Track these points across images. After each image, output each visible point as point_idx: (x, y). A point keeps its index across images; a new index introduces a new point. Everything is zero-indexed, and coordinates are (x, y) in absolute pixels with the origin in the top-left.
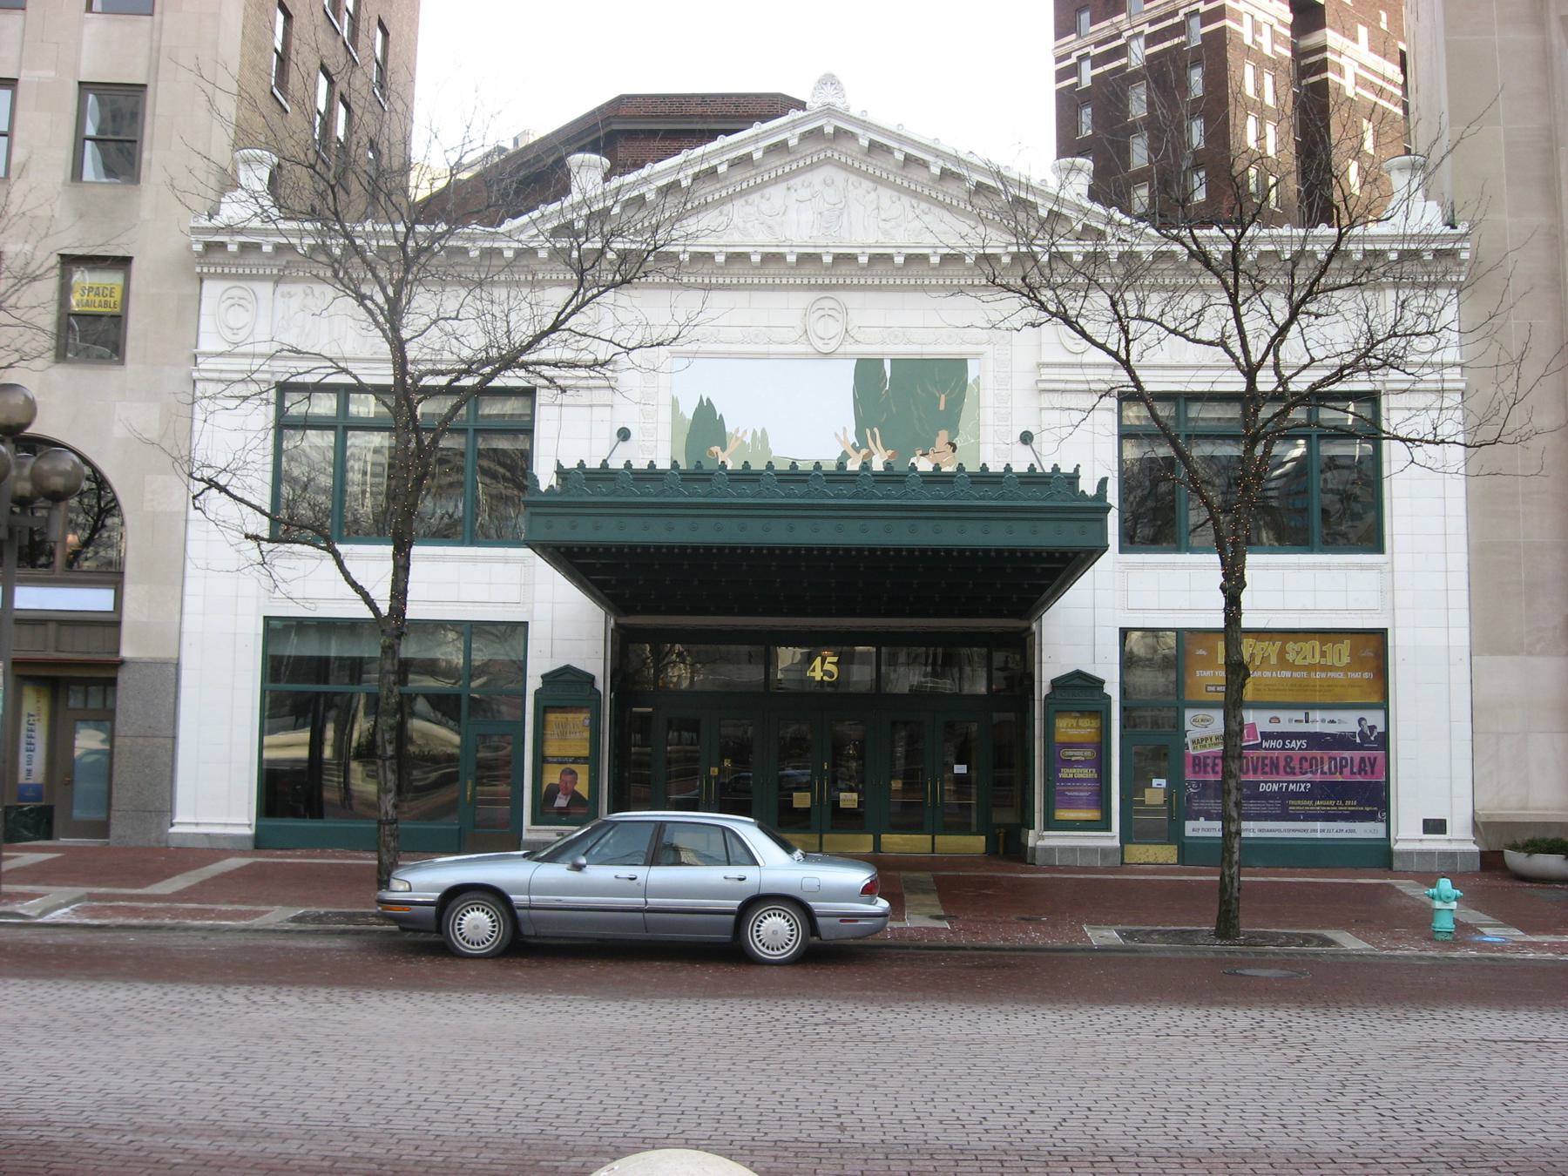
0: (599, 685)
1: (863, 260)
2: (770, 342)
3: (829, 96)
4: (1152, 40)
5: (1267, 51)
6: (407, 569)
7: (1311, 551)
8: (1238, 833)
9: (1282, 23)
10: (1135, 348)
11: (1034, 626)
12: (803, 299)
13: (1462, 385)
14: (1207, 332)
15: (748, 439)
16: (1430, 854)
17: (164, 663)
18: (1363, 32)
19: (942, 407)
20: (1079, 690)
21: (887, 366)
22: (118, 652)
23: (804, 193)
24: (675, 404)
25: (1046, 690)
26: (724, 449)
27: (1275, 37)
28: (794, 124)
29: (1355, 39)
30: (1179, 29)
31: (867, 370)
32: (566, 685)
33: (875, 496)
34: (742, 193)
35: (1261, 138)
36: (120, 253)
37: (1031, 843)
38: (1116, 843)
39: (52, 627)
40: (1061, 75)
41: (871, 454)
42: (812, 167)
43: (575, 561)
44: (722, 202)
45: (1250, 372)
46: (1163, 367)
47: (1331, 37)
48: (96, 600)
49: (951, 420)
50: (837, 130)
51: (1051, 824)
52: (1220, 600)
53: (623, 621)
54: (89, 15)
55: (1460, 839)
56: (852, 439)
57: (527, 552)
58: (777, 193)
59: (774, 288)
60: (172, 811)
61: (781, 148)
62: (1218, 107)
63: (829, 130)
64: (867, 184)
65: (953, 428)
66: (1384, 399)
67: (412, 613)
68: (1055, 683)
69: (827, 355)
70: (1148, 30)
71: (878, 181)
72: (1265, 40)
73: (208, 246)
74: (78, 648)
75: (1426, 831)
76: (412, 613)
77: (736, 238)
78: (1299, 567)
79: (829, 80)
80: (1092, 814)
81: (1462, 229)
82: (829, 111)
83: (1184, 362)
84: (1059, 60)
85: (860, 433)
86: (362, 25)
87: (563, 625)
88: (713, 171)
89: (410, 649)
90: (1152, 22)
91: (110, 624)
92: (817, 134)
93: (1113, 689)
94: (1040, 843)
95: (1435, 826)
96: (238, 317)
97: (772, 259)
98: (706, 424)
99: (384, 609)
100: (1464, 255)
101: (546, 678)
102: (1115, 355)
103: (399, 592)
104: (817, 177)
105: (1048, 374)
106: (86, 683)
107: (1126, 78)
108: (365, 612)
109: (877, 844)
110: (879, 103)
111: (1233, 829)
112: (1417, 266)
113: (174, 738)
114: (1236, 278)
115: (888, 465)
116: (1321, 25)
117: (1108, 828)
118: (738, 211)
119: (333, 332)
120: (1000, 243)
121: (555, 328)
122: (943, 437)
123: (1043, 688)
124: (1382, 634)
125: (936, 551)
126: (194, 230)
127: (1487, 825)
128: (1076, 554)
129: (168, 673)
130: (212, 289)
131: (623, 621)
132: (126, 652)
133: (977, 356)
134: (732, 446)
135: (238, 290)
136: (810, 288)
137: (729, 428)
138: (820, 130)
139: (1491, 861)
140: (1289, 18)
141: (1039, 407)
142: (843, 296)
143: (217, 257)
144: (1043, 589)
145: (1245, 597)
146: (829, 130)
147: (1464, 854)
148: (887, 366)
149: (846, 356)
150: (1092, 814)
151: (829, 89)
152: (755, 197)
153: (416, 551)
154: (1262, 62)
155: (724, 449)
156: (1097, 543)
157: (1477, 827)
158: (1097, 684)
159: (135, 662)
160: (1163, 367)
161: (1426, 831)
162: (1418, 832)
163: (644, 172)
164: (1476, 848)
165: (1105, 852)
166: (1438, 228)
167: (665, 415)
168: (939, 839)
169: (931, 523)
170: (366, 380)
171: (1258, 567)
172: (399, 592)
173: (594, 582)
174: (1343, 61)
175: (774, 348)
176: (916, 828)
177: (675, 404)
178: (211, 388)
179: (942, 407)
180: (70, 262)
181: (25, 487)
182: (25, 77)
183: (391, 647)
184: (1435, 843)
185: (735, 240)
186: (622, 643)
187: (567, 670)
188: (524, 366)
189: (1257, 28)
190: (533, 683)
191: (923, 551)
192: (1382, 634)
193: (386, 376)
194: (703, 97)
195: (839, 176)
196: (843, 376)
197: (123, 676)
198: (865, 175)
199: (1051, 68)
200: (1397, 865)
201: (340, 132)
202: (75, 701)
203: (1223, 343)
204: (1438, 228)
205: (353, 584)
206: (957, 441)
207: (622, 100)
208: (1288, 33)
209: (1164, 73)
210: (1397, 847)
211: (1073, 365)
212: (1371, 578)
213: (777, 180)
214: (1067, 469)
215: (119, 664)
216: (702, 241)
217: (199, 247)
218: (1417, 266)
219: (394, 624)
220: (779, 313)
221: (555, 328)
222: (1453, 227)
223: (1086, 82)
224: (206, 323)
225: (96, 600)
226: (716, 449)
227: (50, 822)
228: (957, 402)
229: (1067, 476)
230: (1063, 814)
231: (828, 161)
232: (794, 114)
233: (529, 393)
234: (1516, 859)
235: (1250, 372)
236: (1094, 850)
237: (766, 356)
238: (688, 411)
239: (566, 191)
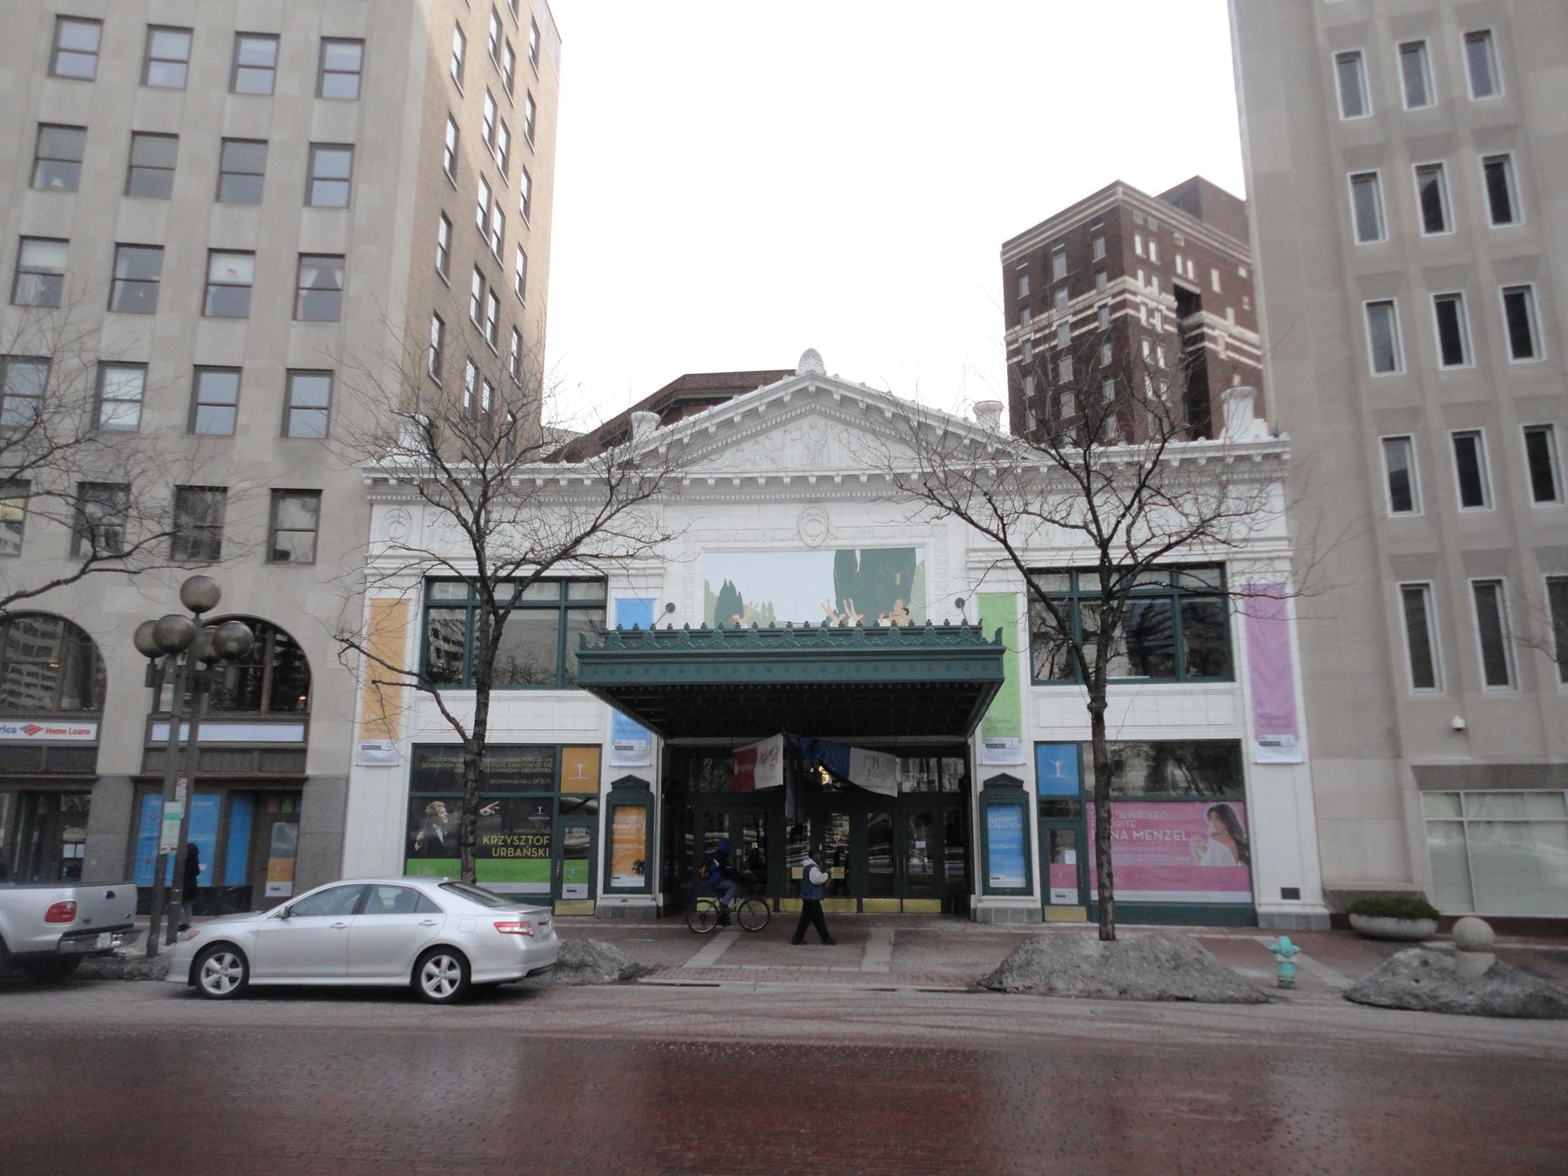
0: (653, 789)
1: (838, 480)
2: (774, 540)
3: (811, 365)
4: (1075, 326)
5: (1159, 329)
6: (486, 705)
7: (1178, 680)
8: (1111, 898)
9: (1169, 309)
10: (1009, 531)
11: (970, 741)
12: (794, 510)
13: (1290, 554)
14: (1076, 519)
15: (759, 609)
17: (337, 778)
18: (1230, 312)
19: (898, 582)
20: (1005, 789)
21: (858, 554)
22: (303, 771)
23: (797, 434)
24: (707, 585)
26: (742, 616)
27: (1165, 319)
28: (787, 386)
29: (1224, 317)
30: (1095, 317)
31: (844, 558)
32: (629, 791)
33: (829, 645)
34: (753, 436)
35: (1157, 393)
38: (1039, 905)
39: (256, 755)
40: (1011, 355)
41: (847, 617)
42: (802, 416)
43: (624, 698)
44: (738, 442)
45: (1104, 544)
47: (1206, 316)
48: (288, 733)
49: (905, 592)
50: (818, 388)
51: (988, 890)
52: (1087, 718)
53: (670, 742)
55: (1312, 904)
56: (834, 607)
57: (584, 693)
58: (777, 435)
59: (776, 502)
61: (778, 403)
62: (1125, 367)
63: (812, 389)
64: (840, 427)
65: (906, 596)
66: (1228, 565)
67: (490, 738)
68: (987, 784)
69: (814, 548)
70: (1072, 319)
71: (848, 424)
72: (1157, 321)
73: (375, 480)
74: (275, 769)
76: (490, 738)
77: (749, 467)
78: (1168, 693)
79: (811, 354)
81: (1284, 437)
82: (812, 375)
83: (1062, 544)
84: (1008, 344)
85: (839, 603)
86: (501, 330)
87: (623, 750)
88: (730, 421)
89: (488, 762)
90: (1074, 314)
91: (298, 752)
92: (804, 391)
93: (1030, 787)
94: (980, 905)
95: (1291, 893)
96: (399, 532)
97: (774, 481)
98: (729, 598)
99: (470, 734)
100: (1286, 457)
101: (616, 785)
102: (996, 536)
103: (481, 722)
104: (805, 423)
105: (973, 556)
106: (280, 796)
107: (1056, 355)
108: (457, 739)
109: (860, 907)
110: (849, 367)
111: (1107, 894)
112: (1261, 467)
113: (343, 834)
114: (1086, 480)
115: (859, 624)
116: (1198, 308)
117: (1031, 893)
118: (748, 449)
119: (442, 540)
120: (906, 461)
121: (594, 529)
122: (899, 604)
123: (977, 787)
125: (839, 685)
127: (1333, 892)
128: (981, 685)
129: (340, 786)
130: (379, 512)
131: (670, 742)
132: (310, 771)
133: (922, 545)
134: (748, 614)
135: (394, 511)
136: (801, 501)
137: (745, 602)
138: (806, 389)
139: (1339, 922)
140: (1175, 305)
141: (959, 579)
143: (382, 489)
144: (967, 713)
145: (1107, 714)
147: (1317, 916)
148: (858, 554)
149: (828, 548)
151: (812, 360)
152: (762, 438)
153: (493, 693)
154: (1156, 339)
155: (742, 616)
156: (996, 676)
157: (1329, 895)
158: (1018, 783)
159: (315, 778)
162: (1277, 897)
163: (681, 423)
164: (1326, 911)
165: (1031, 912)
166: (1266, 437)
167: (700, 595)
168: (906, 902)
169: (872, 665)
170: (464, 573)
171: (499, 699)
172: (481, 722)
173: (641, 714)
174: (1215, 333)
175: (776, 544)
176: (888, 894)
177: (707, 585)
179: (898, 582)
180: (279, 494)
181: (210, 650)
183: (474, 762)
184: (1291, 907)
185: (749, 470)
186: (673, 762)
187: (630, 778)
188: (575, 557)
189: (1151, 313)
190: (606, 788)
191: (829, 685)
193: (471, 569)
194: (742, 374)
195: (821, 422)
196: (828, 561)
197: (308, 790)
198: (839, 420)
199: (1002, 351)
200: (1262, 924)
201: (486, 404)
202: (272, 809)
203: (1085, 527)
204: (1266, 437)
205: (452, 720)
206: (909, 607)
207: (685, 378)
208: (1174, 316)
209: (1083, 350)
210: (1261, 910)
212: (1225, 701)
213: (776, 426)
214: (974, 622)
215: (305, 780)
217: (369, 482)
218: (1261, 467)
219: (476, 745)
220: (782, 518)
221: (594, 529)
222: (1276, 436)
223: (1029, 360)
225: (288, 733)
226: (736, 617)
227: (249, 899)
228: (908, 580)
229: (973, 628)
231: (813, 411)
232: (787, 379)
234: (1358, 921)
235: (1104, 544)
237: (772, 550)
238: (716, 590)
239: (630, 439)
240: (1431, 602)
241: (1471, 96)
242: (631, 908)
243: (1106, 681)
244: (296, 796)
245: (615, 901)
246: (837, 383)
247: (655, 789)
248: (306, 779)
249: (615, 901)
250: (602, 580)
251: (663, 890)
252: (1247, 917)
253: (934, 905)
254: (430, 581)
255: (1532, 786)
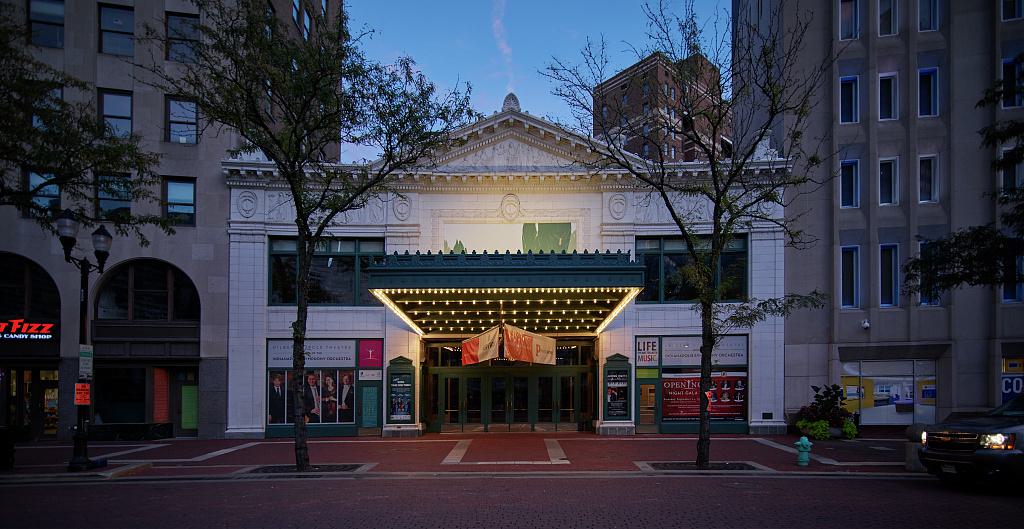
16: (766, 427)
25: (605, 362)
36: (191, 175)
37: (597, 426)
46: (655, 225)
54: (166, 62)
55: (778, 421)
60: (227, 424)
63: (511, 121)
73: (231, 171)
75: (763, 418)
80: (408, 417)
96: (248, 205)
104: (506, 144)
113: (227, 392)
123: (602, 362)
124: (382, 340)
126: (223, 164)
129: (224, 362)
130: (235, 192)
136: (612, 190)
142: (256, 192)
146: (511, 121)
147: (780, 427)
150: (408, 417)
159: (206, 359)
160: (655, 225)
161: (763, 418)
171: (313, 312)
178: (237, 237)
182: (136, 89)
184: (768, 423)
192: (382, 340)
195: (515, 143)
197: (202, 365)
211: (616, 224)
216: (439, 169)
224: (233, 208)
230: (395, 417)
233: (744, 236)
236: (623, 428)
240: (858, 258)
241: (881, 75)
242: (403, 431)
243: (703, 336)
244: (196, 371)
245: (393, 428)
246: (527, 118)
247: (417, 364)
248: (201, 359)
249: (393, 428)
250: (381, 240)
251: (421, 421)
252: (351, 282)
253: (188, 393)
254: (273, 239)
255: (753, 479)
